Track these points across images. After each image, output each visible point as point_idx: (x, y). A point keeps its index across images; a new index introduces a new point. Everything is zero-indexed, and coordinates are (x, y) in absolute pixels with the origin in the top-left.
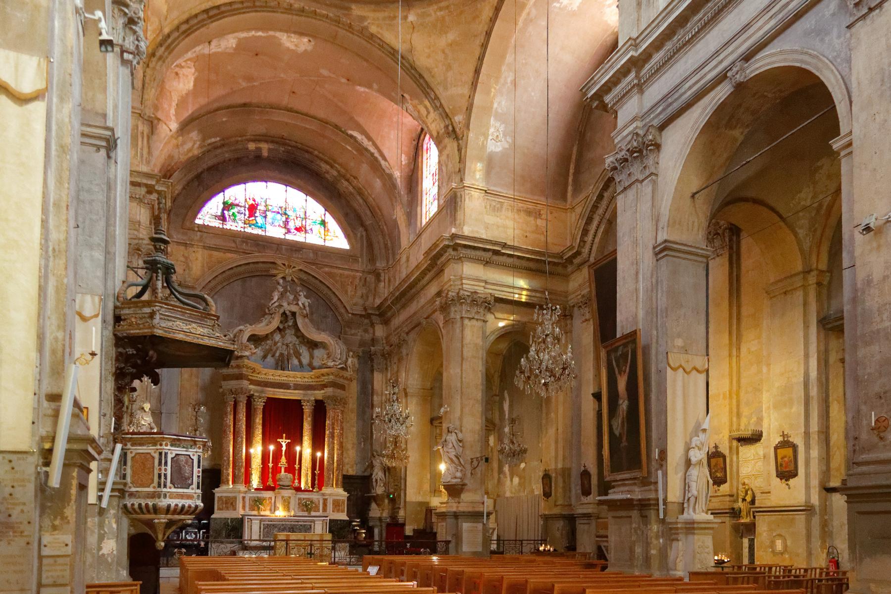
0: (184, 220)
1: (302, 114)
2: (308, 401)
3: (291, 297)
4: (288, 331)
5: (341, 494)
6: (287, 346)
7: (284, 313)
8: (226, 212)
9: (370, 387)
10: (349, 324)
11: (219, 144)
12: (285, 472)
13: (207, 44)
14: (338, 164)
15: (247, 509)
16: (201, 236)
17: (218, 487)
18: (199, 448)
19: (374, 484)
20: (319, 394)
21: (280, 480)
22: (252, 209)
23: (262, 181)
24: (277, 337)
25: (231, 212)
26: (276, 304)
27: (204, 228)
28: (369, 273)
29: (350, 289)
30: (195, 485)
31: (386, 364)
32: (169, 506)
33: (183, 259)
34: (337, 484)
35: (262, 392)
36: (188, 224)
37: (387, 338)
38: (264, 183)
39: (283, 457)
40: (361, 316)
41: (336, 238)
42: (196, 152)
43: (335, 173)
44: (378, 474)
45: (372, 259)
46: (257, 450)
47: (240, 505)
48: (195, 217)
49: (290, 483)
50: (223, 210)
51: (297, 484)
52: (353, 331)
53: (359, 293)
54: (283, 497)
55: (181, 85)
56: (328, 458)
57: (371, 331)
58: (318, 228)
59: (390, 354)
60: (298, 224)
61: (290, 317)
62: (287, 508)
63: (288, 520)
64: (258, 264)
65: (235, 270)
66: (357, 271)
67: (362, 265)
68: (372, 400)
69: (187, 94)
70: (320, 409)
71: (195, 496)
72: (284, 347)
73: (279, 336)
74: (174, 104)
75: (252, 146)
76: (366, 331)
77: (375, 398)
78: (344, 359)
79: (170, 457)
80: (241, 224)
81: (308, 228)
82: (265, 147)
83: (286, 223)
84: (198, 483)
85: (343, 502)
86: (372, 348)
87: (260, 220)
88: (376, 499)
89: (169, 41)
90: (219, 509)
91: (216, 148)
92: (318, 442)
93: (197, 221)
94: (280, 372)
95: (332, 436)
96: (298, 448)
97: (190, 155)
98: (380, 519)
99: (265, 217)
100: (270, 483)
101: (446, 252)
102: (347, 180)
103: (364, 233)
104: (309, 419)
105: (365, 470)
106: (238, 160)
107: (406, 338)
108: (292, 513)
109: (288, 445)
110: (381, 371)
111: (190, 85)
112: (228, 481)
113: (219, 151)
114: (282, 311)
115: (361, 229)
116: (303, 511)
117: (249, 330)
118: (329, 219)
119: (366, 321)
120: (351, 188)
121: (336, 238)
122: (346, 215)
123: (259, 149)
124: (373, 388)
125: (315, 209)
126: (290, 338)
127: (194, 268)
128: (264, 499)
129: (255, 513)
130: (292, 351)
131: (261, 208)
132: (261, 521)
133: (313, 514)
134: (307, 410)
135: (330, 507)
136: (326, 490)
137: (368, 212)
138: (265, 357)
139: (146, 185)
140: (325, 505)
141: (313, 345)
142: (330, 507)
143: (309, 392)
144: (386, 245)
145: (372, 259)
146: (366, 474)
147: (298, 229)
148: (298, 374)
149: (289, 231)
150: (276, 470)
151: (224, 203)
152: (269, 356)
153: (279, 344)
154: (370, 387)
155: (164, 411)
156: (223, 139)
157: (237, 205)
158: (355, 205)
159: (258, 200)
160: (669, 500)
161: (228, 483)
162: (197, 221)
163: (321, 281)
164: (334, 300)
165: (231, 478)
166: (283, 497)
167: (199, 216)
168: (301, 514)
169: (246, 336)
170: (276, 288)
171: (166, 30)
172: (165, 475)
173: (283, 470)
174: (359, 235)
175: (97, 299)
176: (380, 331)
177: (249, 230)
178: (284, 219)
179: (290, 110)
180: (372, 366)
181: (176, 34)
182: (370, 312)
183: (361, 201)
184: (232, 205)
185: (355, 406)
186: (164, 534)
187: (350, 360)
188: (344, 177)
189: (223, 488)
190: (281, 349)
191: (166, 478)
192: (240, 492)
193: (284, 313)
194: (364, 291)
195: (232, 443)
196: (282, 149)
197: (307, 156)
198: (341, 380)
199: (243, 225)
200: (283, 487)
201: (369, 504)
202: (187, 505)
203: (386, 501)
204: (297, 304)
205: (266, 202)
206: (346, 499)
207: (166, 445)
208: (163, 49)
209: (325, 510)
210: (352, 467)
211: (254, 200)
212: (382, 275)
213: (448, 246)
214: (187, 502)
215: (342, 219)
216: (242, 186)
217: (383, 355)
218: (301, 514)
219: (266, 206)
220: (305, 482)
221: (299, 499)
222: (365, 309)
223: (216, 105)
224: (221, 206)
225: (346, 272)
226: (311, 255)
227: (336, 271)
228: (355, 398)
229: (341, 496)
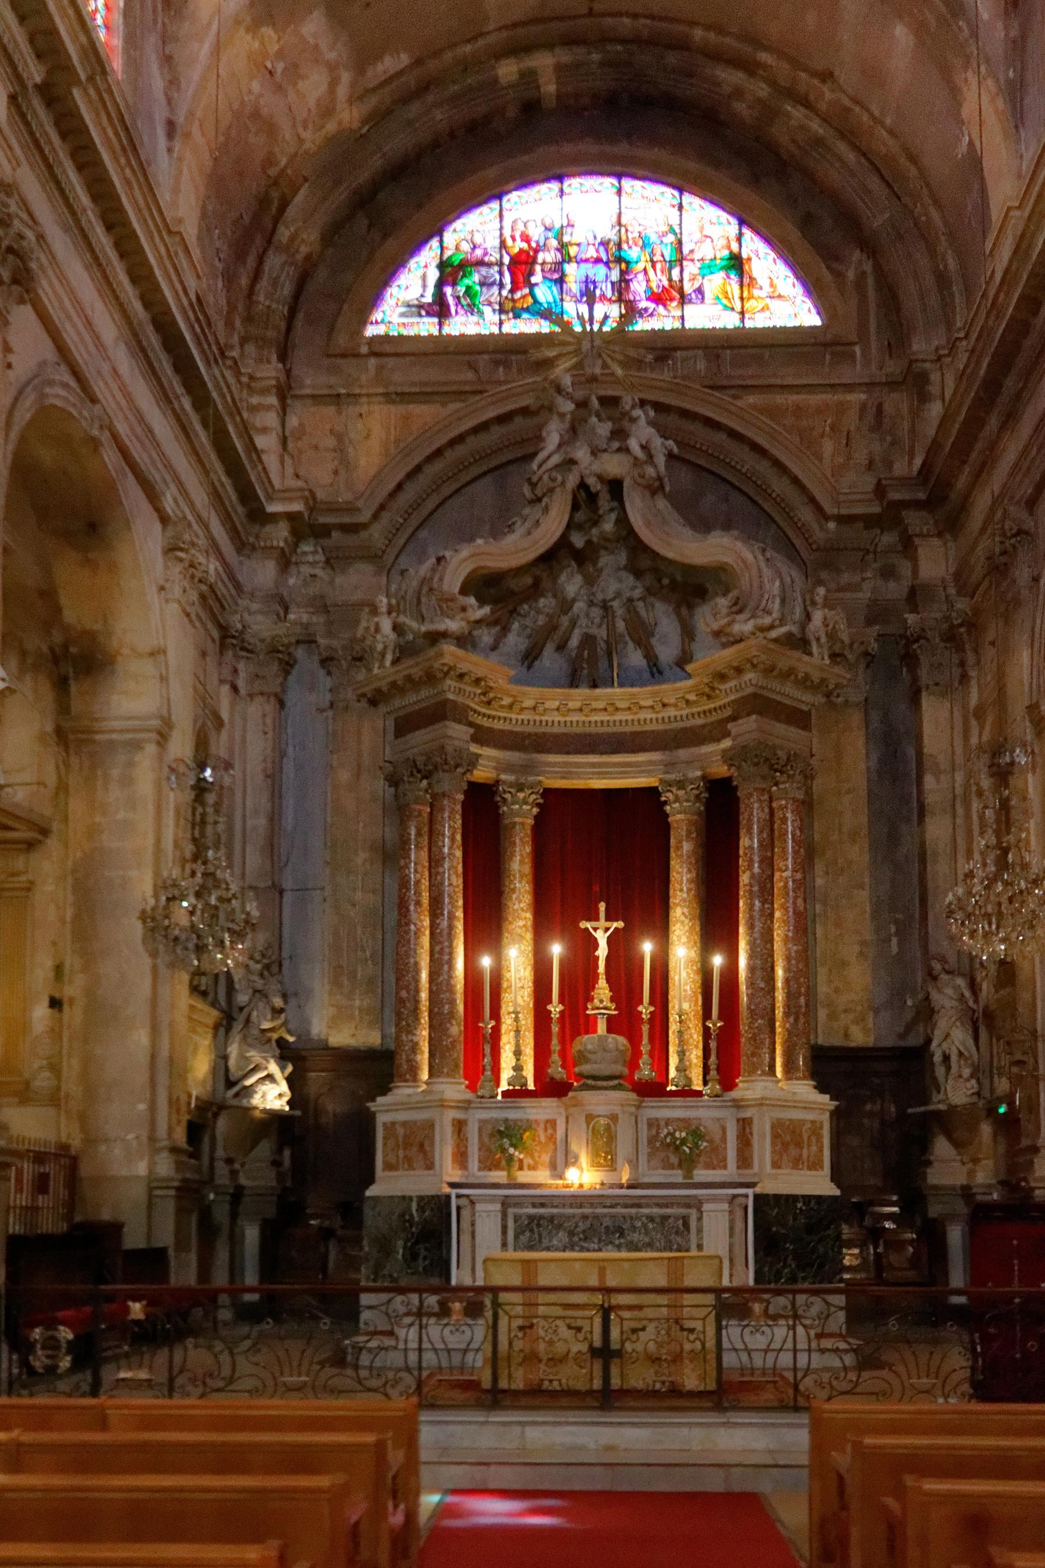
0: (332, 329)
1: (782, 346)
2: (681, 784)
3: (604, 429)
4: (605, 560)
5: (808, 1101)
6: (605, 606)
7: (583, 485)
8: (448, 290)
9: (911, 752)
11: (411, 80)
12: (610, 1030)
15: (474, 1163)
16: (380, 368)
19: (940, 1071)
20: (712, 758)
21: (583, 1057)
22: (522, 265)
23: (547, 180)
24: (571, 584)
25: (461, 289)
26: (556, 459)
27: (390, 348)
28: (892, 385)
29: (828, 447)
31: (962, 664)
33: (331, 442)
34: (790, 1068)
36: (341, 341)
37: (957, 576)
38: (555, 186)
39: (602, 982)
41: (784, 303)
42: (349, 116)
43: (762, 90)
44: (951, 1036)
45: (897, 337)
46: (516, 960)
47: (445, 1152)
48: (364, 320)
49: (621, 1069)
50: (440, 284)
51: (646, 1072)
52: (846, 578)
53: (861, 456)
54: (589, 1118)
56: (751, 969)
57: (905, 568)
58: (715, 283)
59: (973, 624)
60: (658, 280)
61: (604, 503)
62: (606, 1154)
63: (614, 1202)
65: (472, 442)
66: (849, 388)
67: (867, 363)
68: (920, 792)
70: (720, 805)
72: (596, 612)
73: (578, 579)
76: (888, 573)
77: (929, 781)
78: (798, 613)
80: (490, 316)
81: (688, 288)
82: (544, 62)
83: (622, 287)
85: (816, 1129)
86: (911, 618)
87: (545, 293)
88: (949, 1123)
90: (388, 1167)
91: (405, 99)
92: (717, 925)
94: (582, 693)
95: (765, 890)
96: (647, 947)
97: (331, 127)
98: (966, 1192)
99: (561, 281)
100: (556, 1070)
102: (805, 102)
103: (868, 267)
104: (687, 847)
105: (909, 1028)
106: (473, 127)
107: (1029, 524)
108: (625, 1177)
110: (944, 691)
112: (413, 1070)
113: (414, 109)
114: (572, 481)
115: (857, 255)
116: (668, 1166)
117: (461, 563)
118: (753, 245)
119: (888, 539)
120: (816, 126)
121: (784, 303)
122: (807, 223)
123: (529, 77)
124: (920, 754)
125: (707, 226)
126: (615, 581)
127: (363, 462)
128: (529, 1125)
129: (499, 1176)
130: (621, 625)
131: (548, 257)
132: (506, 1203)
133: (701, 1175)
134: (681, 814)
135: (763, 1149)
136: (750, 1088)
137: (874, 183)
138: (530, 657)
140: (745, 1142)
141: (689, 588)
142: (763, 1149)
143: (682, 754)
144: (942, 280)
145: (897, 337)
146: (913, 1041)
147: (658, 298)
148: (644, 694)
150: (577, 1021)
151: (442, 265)
152: (549, 650)
153: (580, 606)
154: (911, 752)
155: (288, 884)
156: (418, 62)
157: (481, 263)
158: (833, 176)
159: (536, 234)
161: (415, 1078)
163: (733, 434)
164: (780, 486)
165: (423, 1058)
166: (589, 1118)
167: (377, 316)
168: (659, 1176)
169: (453, 580)
170: (550, 408)
173: (602, 1027)
174: (851, 275)
176: (934, 562)
177: (514, 327)
178: (615, 275)
180: (915, 680)
182: (894, 495)
183: (851, 157)
185: (864, 819)
187: (818, 616)
189: (401, 1092)
190: (586, 621)
192: (442, 1104)
193: (583, 485)
194: (877, 447)
195: (425, 940)
196: (596, 57)
197: (672, 59)
198: (789, 689)
199: (496, 318)
200: (595, 1081)
201: (924, 1145)
203: (986, 1129)
204: (625, 450)
205: (559, 237)
206: (826, 1118)
209: (744, 1161)
210: (861, 1020)
211: (526, 238)
212: (935, 377)
215: (794, 234)
216: (495, 205)
217: (951, 637)
218: (659, 1176)
219: (562, 247)
220: (686, 1057)
221: (652, 1123)
224: (433, 275)
225: (815, 399)
226: (701, 365)
227: (780, 399)
228: (864, 793)
229: (807, 1107)
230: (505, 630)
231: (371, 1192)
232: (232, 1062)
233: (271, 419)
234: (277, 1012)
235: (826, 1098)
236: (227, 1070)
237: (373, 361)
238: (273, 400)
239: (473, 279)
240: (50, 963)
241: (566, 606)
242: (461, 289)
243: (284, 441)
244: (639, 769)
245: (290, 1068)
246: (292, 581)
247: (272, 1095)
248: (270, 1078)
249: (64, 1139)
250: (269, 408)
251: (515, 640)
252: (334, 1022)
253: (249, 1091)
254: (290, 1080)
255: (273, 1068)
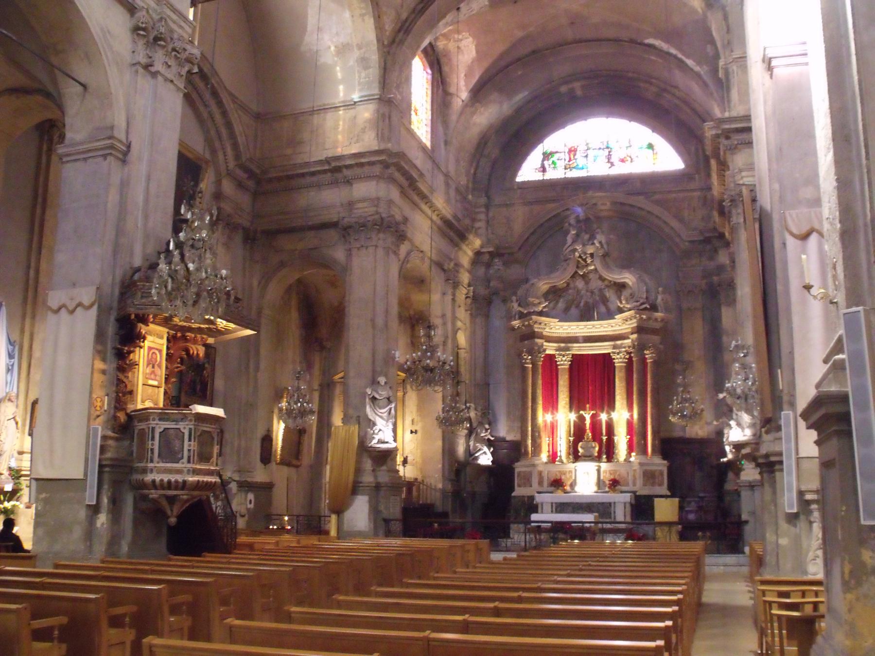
3: (587, 237)
8: (546, 163)
10: (687, 254)
13: (455, 12)
14: (656, 79)
17: (518, 461)
18: (191, 420)
25: (550, 162)
27: (526, 185)
30: (185, 459)
32: (154, 481)
35: (568, 349)
40: (700, 242)
41: (667, 159)
48: (515, 175)
50: (543, 160)
55: (466, 57)
64: (624, 205)
69: (472, 62)
71: (185, 470)
72: (589, 294)
74: (462, 75)
75: (564, 89)
79: (158, 431)
82: (577, 85)
83: (609, 157)
84: (189, 457)
89: (407, 24)
90: (519, 486)
92: (630, 407)
93: (519, 179)
96: (603, 417)
101: (719, 143)
109: (593, 417)
111: (474, 53)
112: (526, 453)
119: (708, 247)
120: (677, 102)
121: (667, 159)
123: (572, 91)
130: (598, 298)
131: (581, 149)
138: (567, 309)
139: (380, 162)
143: (619, 342)
149: (612, 164)
151: (544, 154)
152: (573, 306)
160: (802, 454)
162: (519, 179)
171: (404, 16)
172: (152, 450)
175: (95, 288)
179: (580, 41)
181: (413, 16)
182: (707, 235)
183: (689, 111)
184: (552, 154)
186: (172, 511)
188: (665, 90)
191: (152, 453)
202: (173, 480)
207: (154, 420)
208: (401, 34)
213: (717, 136)
214: (180, 478)
222: (701, 232)
223: (503, 63)
225: (681, 195)
229: (659, 465)
230: (557, 302)
231: (513, 494)
232: (471, 448)
233: (482, 216)
234: (487, 430)
235: (666, 462)
236: (700, 241)
237: (519, 191)
238: (483, 210)
239: (556, 156)
240: (410, 419)
241: (578, 292)
242: (550, 162)
243: (488, 222)
244: (605, 348)
245: (492, 449)
246: (491, 272)
247: (485, 459)
248: (485, 453)
249: (317, 359)
250: (481, 212)
251: (561, 305)
252: (508, 432)
253: (477, 458)
254: (492, 453)
255: (485, 449)
